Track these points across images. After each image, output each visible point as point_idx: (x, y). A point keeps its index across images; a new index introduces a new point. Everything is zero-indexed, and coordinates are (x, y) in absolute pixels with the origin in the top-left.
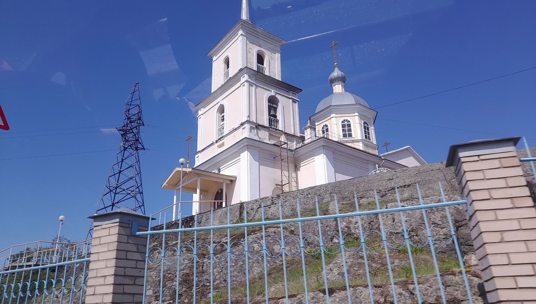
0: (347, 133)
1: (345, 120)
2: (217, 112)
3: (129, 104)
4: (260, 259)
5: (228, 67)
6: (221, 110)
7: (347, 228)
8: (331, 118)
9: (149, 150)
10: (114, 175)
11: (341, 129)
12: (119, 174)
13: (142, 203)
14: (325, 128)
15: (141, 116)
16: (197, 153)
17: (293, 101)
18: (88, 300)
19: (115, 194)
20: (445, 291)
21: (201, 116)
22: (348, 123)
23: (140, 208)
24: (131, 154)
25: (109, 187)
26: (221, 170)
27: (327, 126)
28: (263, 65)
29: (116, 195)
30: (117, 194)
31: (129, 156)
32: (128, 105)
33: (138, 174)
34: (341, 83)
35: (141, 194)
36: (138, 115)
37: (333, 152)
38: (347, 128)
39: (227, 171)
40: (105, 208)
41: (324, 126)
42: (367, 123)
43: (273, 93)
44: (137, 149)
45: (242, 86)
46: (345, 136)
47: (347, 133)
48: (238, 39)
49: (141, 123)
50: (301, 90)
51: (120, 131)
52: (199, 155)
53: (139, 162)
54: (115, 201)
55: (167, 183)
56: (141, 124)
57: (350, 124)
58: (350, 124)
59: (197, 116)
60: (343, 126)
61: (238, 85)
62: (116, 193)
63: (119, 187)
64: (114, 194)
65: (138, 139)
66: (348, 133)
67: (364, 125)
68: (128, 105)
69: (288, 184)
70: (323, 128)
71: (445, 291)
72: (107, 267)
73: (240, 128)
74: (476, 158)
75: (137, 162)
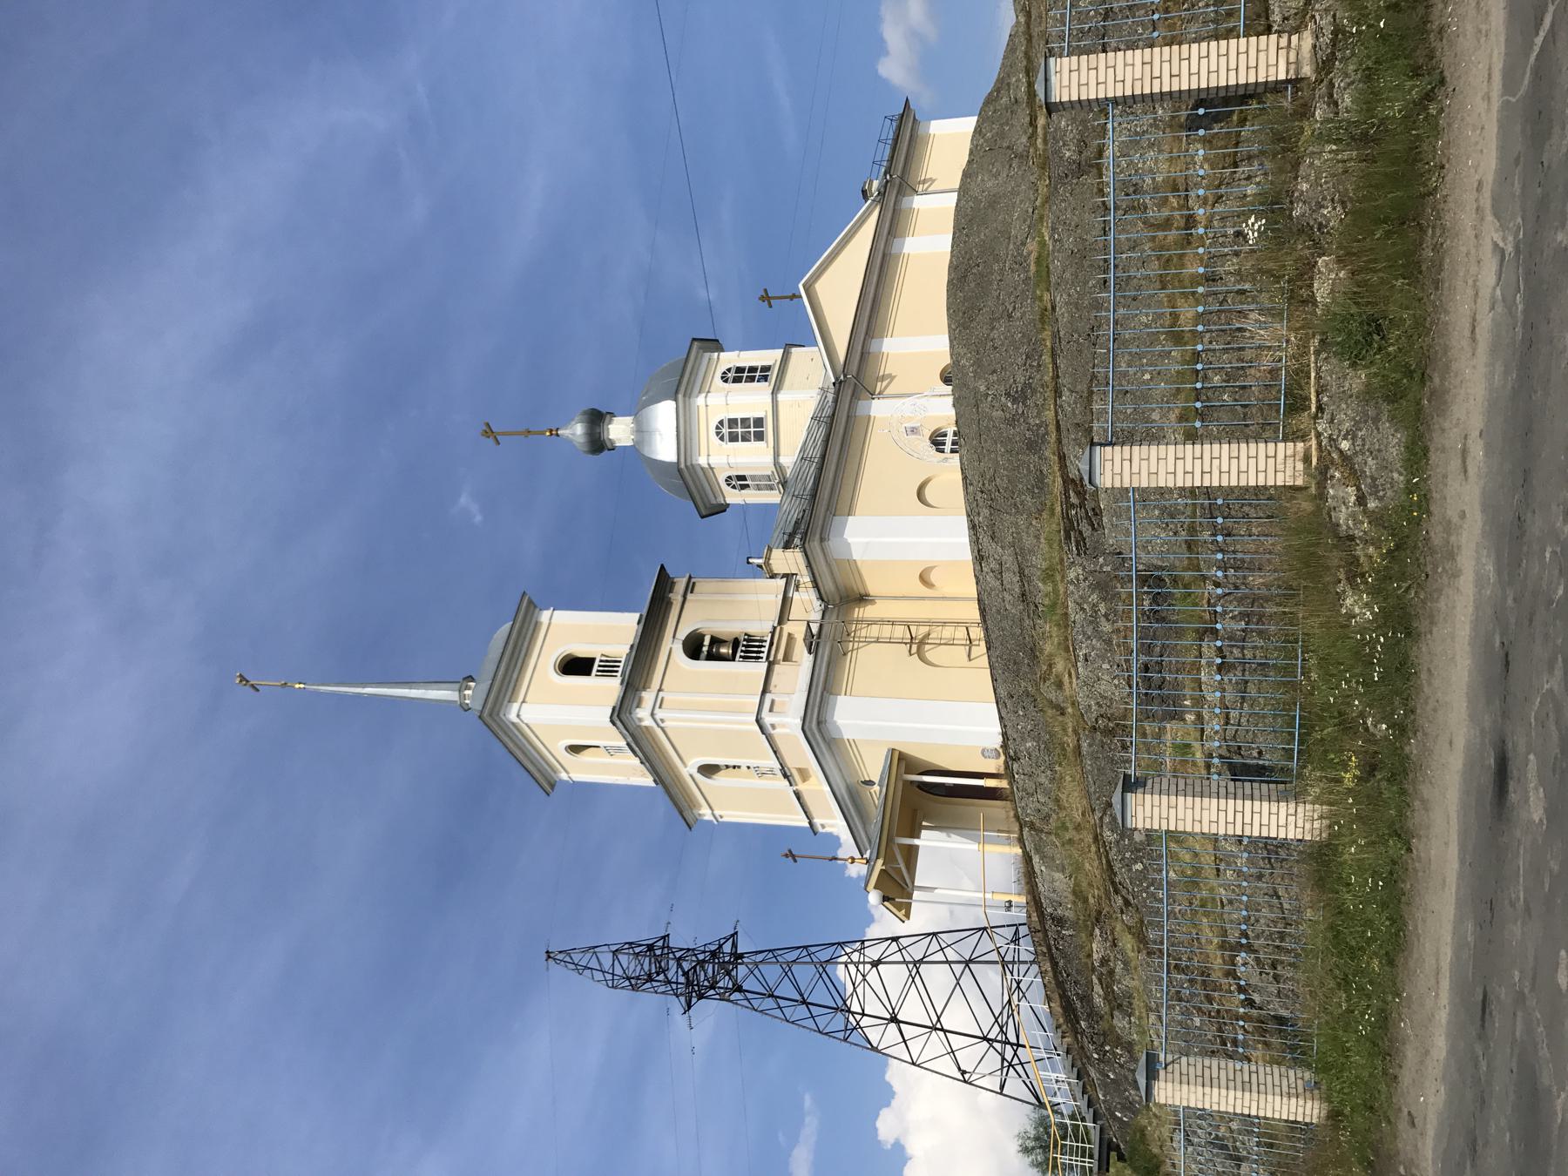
2: (709, 778)
3: (609, 977)
6: (709, 770)
12: (901, 1024)
13: (890, 941)
14: (734, 483)
16: (813, 830)
19: (863, 1014)
22: (726, 424)
25: (849, 1032)
26: (868, 779)
27: (730, 477)
29: (866, 1012)
32: (613, 980)
33: (809, 955)
34: (605, 427)
36: (641, 952)
37: (834, 515)
39: (873, 767)
40: (905, 1041)
41: (729, 485)
42: (724, 373)
43: (678, 649)
44: (737, 957)
45: (662, 725)
50: (662, 567)
51: (693, 1003)
52: (817, 821)
53: (774, 950)
54: (799, 998)
55: (900, 911)
56: (666, 945)
57: (729, 420)
59: (715, 822)
60: (733, 438)
62: (861, 1011)
63: (896, 1011)
64: (865, 1017)
66: (754, 427)
67: (731, 380)
70: (734, 487)
72: (1196, 1092)
75: (775, 957)
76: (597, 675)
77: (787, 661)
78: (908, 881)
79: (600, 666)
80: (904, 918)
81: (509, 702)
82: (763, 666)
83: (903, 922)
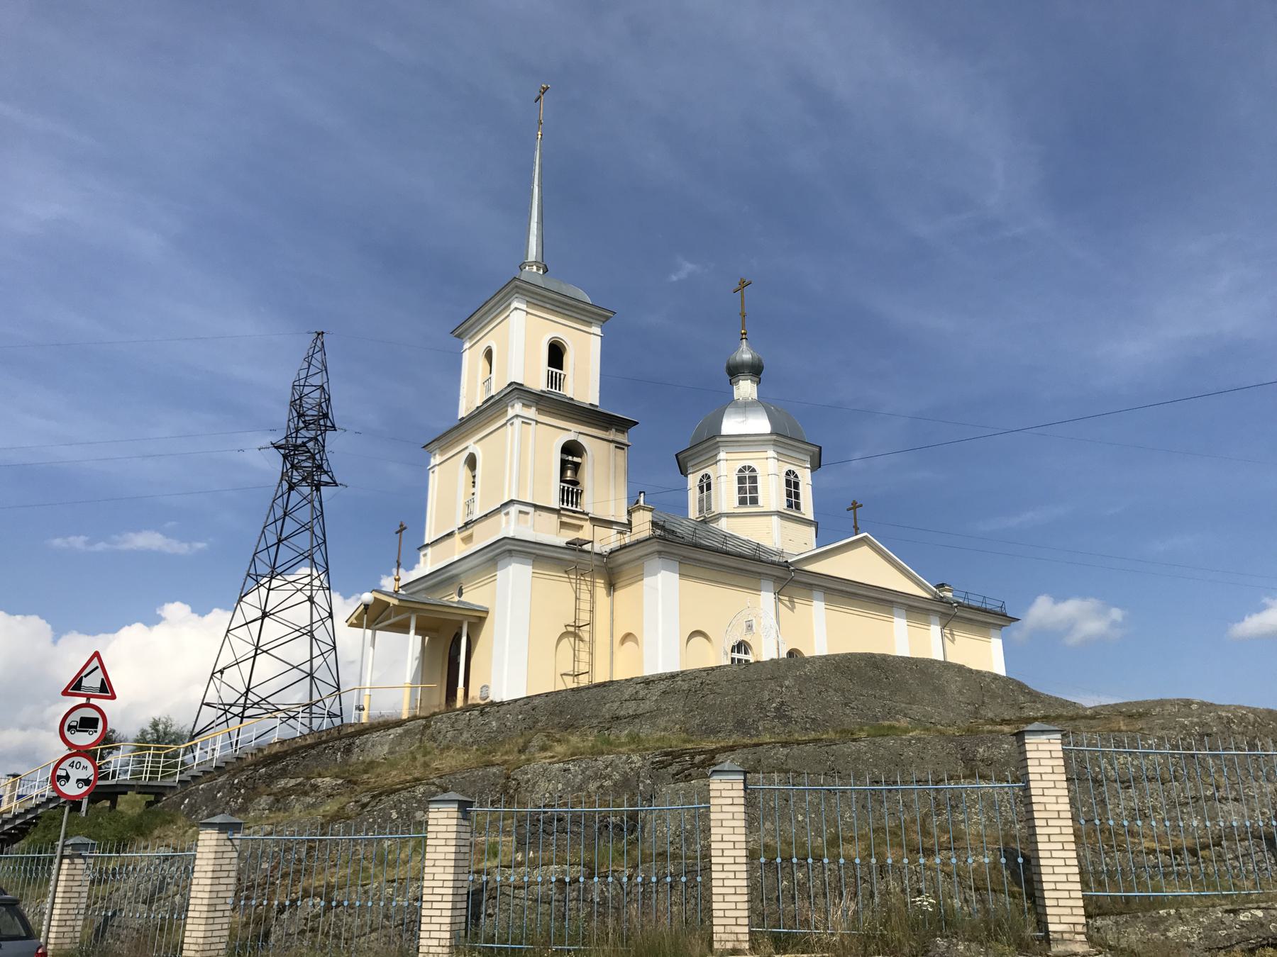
0: (748, 495)
1: (740, 469)
3: (302, 382)
4: (394, 829)
5: (491, 373)
9: (346, 487)
10: (267, 548)
11: (736, 486)
13: (329, 611)
14: (705, 481)
15: (328, 410)
17: (616, 447)
18: (185, 953)
19: (269, 590)
21: (437, 468)
22: (753, 474)
23: (323, 623)
26: (464, 591)
27: (709, 477)
28: (561, 369)
29: (271, 591)
30: (272, 589)
31: (297, 532)
32: (300, 386)
35: (327, 592)
38: (748, 485)
39: (474, 596)
40: (247, 624)
41: (703, 476)
44: (317, 486)
45: (508, 424)
47: (748, 495)
48: (509, 316)
49: (329, 424)
50: (636, 423)
52: (429, 551)
53: (323, 517)
60: (741, 480)
61: (503, 421)
62: (271, 588)
65: (322, 464)
68: (300, 386)
69: (588, 626)
70: (701, 481)
72: (207, 865)
73: (500, 511)
74: (437, 810)
75: (317, 517)
76: (548, 371)
77: (560, 525)
78: (380, 625)
79: (556, 373)
80: (349, 622)
81: (527, 301)
82: (556, 505)
83: (346, 622)
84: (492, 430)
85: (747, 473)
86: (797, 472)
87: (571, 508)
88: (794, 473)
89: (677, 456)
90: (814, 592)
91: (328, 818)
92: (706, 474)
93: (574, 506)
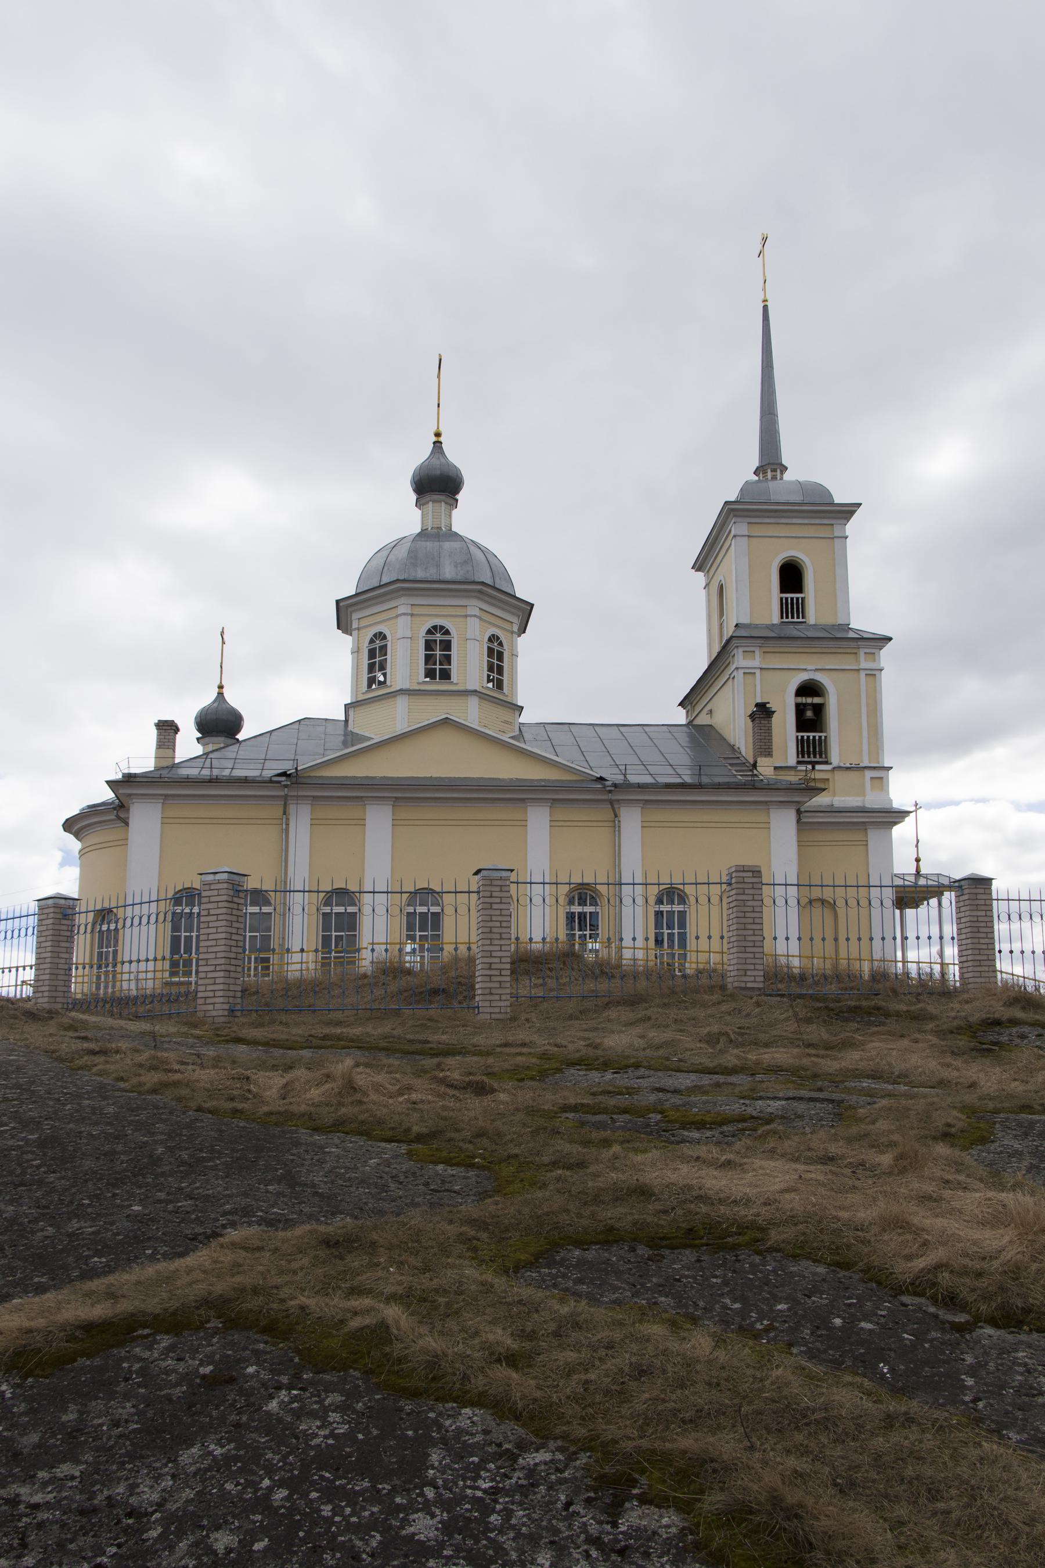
0: (438, 667)
1: (429, 630)
7: (464, 1165)
8: (397, 616)
20: (777, 1136)
22: (446, 638)
24: (16, 986)
27: (385, 637)
41: (375, 635)
46: (430, 674)
47: (438, 667)
58: (449, 642)
60: (429, 645)
70: (372, 641)
71: (777, 1136)
84: (499, 614)
85: (438, 636)
86: (503, 638)
87: (809, 760)
88: (498, 638)
89: (338, 602)
90: (529, 808)
91: (42, 1474)
92: (381, 633)
93: (806, 756)
